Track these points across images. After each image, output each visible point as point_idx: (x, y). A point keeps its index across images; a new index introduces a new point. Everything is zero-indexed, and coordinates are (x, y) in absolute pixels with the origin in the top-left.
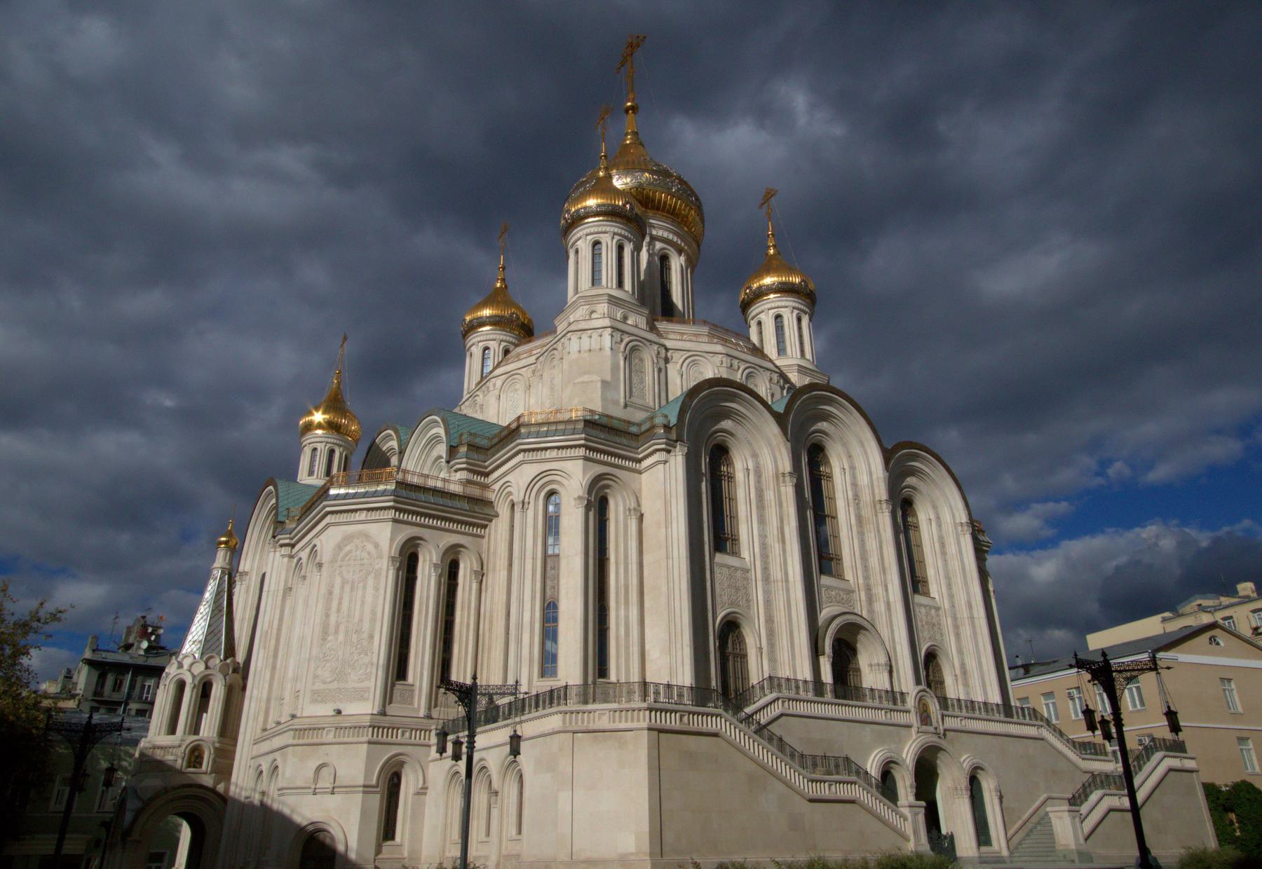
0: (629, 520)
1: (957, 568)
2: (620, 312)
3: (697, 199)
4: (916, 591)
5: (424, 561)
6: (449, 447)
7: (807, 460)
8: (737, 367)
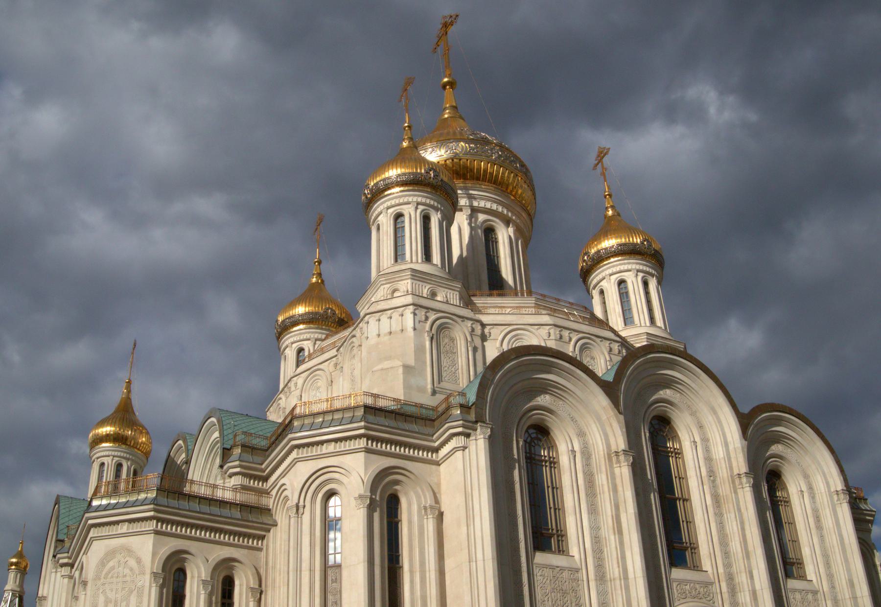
0: (425, 520)
1: (835, 542)
2: (427, 288)
3: (523, 165)
4: (788, 575)
5: (193, 577)
6: (222, 449)
7: (648, 434)
8: (567, 339)
